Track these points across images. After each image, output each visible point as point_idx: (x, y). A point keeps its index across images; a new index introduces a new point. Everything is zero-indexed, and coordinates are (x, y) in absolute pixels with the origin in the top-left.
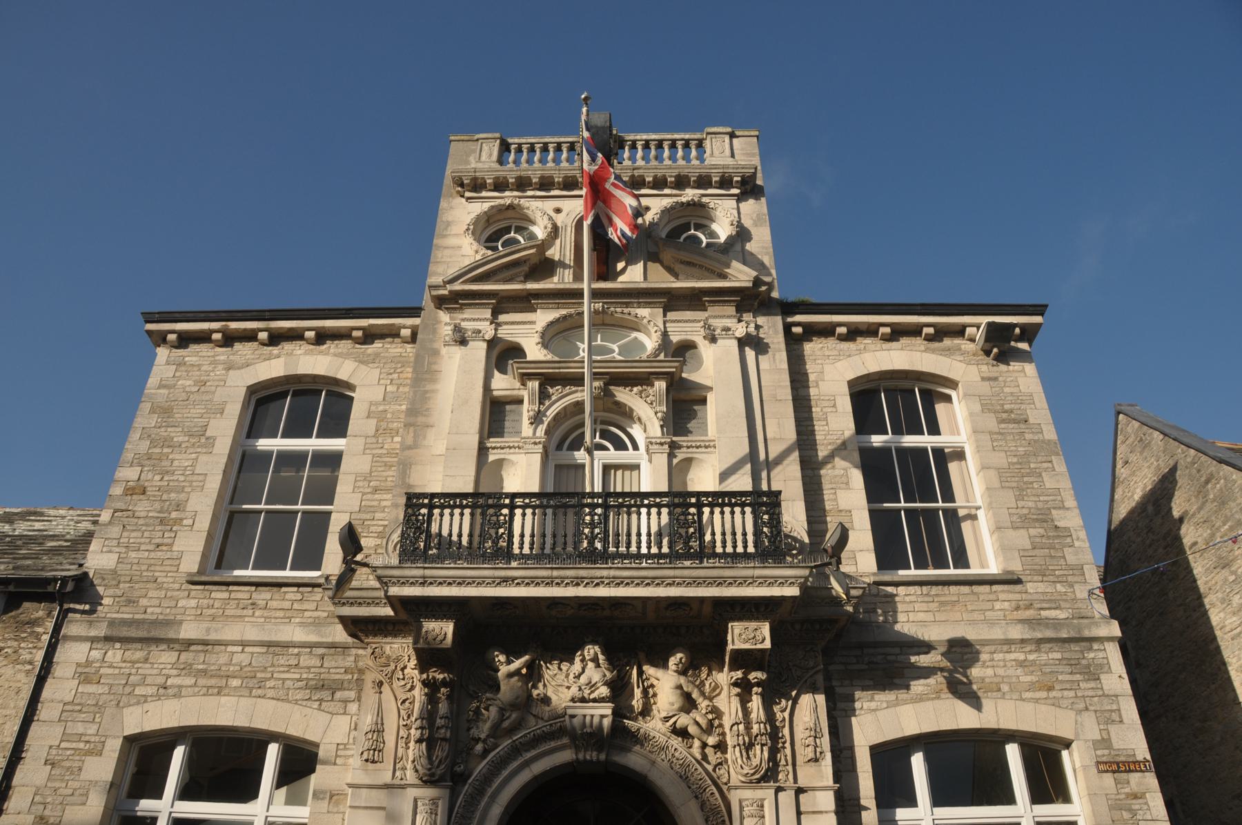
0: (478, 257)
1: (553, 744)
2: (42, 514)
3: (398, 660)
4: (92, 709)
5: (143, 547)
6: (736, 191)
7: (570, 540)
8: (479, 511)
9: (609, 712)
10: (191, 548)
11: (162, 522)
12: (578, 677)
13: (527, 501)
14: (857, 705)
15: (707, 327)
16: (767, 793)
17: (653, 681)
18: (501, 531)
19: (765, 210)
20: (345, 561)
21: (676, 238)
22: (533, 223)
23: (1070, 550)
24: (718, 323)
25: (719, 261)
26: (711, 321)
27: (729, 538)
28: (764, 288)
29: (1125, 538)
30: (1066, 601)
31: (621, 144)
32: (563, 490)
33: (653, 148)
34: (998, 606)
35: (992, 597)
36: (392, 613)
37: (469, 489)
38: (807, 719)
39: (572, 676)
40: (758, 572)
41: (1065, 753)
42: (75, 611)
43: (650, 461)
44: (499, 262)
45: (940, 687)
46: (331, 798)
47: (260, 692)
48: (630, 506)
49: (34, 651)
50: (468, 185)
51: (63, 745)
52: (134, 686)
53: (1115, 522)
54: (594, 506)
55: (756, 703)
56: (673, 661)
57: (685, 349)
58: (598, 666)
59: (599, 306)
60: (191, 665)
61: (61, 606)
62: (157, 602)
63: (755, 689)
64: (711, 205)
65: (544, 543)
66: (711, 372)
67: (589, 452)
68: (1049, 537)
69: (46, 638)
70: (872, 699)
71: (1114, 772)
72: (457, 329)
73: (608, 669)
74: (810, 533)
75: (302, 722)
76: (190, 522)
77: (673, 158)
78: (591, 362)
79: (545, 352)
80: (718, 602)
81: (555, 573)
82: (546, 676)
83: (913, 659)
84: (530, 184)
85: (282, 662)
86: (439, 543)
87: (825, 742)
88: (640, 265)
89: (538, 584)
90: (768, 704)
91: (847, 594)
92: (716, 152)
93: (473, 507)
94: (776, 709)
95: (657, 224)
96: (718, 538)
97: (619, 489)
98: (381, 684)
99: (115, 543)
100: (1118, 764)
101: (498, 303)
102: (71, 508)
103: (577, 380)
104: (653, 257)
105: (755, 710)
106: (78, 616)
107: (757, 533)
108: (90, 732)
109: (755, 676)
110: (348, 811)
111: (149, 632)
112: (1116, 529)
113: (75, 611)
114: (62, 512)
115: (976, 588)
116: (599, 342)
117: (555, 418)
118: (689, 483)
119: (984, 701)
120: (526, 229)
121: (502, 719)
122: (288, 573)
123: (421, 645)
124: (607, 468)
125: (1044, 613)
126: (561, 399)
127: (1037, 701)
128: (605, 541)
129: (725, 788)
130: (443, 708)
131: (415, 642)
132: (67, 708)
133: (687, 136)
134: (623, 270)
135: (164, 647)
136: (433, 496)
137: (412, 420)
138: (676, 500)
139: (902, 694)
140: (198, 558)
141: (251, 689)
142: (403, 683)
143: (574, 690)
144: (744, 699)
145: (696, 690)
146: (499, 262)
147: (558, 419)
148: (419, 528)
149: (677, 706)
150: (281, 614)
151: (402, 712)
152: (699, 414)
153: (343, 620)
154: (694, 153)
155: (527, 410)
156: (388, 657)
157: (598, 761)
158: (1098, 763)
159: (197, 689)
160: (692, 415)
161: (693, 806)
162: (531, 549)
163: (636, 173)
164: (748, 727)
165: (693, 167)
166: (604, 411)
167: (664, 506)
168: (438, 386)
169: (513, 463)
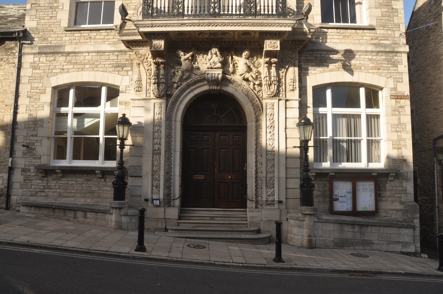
1: (201, 84)
2: (3, 8)
3: (145, 55)
4: (39, 78)
5: (45, 18)
7: (206, 8)
9: (221, 72)
10: (64, 17)
11: (51, 8)
12: (210, 60)
14: (309, 72)
16: (275, 101)
17: (236, 61)
20: (122, 19)
23: (396, 17)
27: (266, 8)
29: (419, 15)
30: (391, 37)
34: (365, 38)
35: (363, 35)
36: (141, 38)
38: (291, 76)
39: (207, 60)
40: (276, 21)
41: (380, 92)
42: (25, 44)
45: (340, 66)
46: (125, 104)
47: (97, 69)
49: (14, 59)
51: (32, 91)
52: (52, 69)
53: (417, 8)
55: (273, 70)
56: (244, 54)
58: (217, 56)
60: (71, 61)
61: (20, 42)
62: (55, 39)
63: (273, 65)
65: (196, 10)
68: (389, 12)
69: (17, 54)
70: (315, 70)
71: (396, 99)
73: (220, 57)
74: (297, 7)
75: (113, 79)
76: (62, 7)
81: (201, 21)
82: (198, 60)
83: (331, 56)
85: (103, 58)
86: (157, 11)
87: (297, 84)
90: (278, 70)
91: (309, 31)
94: (280, 72)
96: (262, 8)
98: (139, 64)
99: (34, 17)
100: (398, 96)
102: (14, 5)
105: (273, 72)
106: (27, 45)
107: (277, 6)
108: (40, 86)
109: (274, 60)
110: (132, 108)
111: (54, 50)
112: (416, 11)
113: (25, 44)
114: (11, 6)
115: (358, 31)
119: (355, 73)
121: (183, 75)
122: (101, 26)
123: (153, 49)
125: (382, 42)
127: (373, 73)
128: (219, 9)
129: (261, 99)
130: (162, 72)
131: (151, 48)
132: (30, 78)
135: (60, 55)
139: (326, 69)
140: (67, 21)
141: (93, 68)
142: (147, 63)
143: (208, 65)
144: (269, 69)
148: (149, 5)
149: (245, 70)
150: (101, 41)
151: (148, 74)
153: (124, 41)
156: (141, 55)
157: (217, 90)
158: (391, 96)
159: (74, 69)
161: (250, 105)
162: (192, 12)
164: (270, 78)
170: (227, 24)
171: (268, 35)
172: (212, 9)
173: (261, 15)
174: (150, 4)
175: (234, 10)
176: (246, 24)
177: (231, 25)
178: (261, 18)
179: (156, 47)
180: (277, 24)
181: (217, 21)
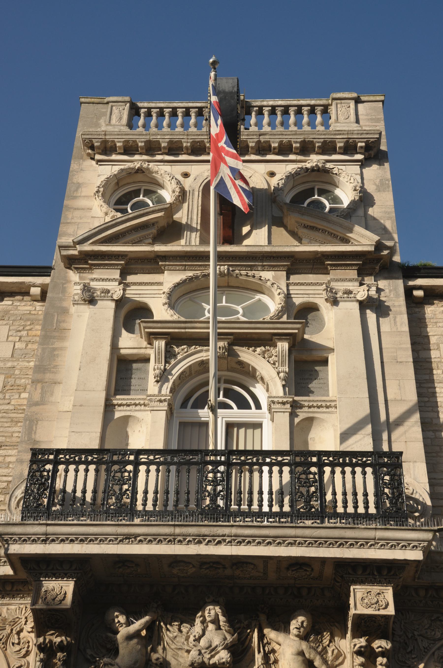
0: (108, 219)
3: (14, 622)
6: (359, 157)
7: (193, 497)
8: (104, 467)
12: (198, 640)
13: (151, 457)
15: (329, 289)
18: (125, 487)
19: (388, 175)
21: (299, 202)
22: (162, 187)
24: (340, 287)
25: (341, 226)
26: (333, 284)
27: (350, 498)
28: (386, 252)
31: (248, 109)
32: (187, 447)
33: (279, 113)
37: (95, 445)
39: (192, 638)
40: (380, 534)
43: (272, 420)
44: (128, 224)
48: (252, 465)
50: (98, 147)
54: (217, 464)
56: (294, 624)
57: (307, 311)
58: (219, 628)
59: (224, 269)
63: (380, 660)
64: (335, 171)
66: (333, 334)
67: (213, 410)
72: (86, 288)
77: (298, 124)
78: (216, 322)
79: (172, 312)
80: (341, 564)
81: (178, 530)
82: (166, 638)
84: (159, 149)
86: (63, 500)
88: (265, 229)
89: (160, 542)
92: (341, 118)
93: (98, 463)
95: (281, 189)
96: (339, 497)
97: (241, 448)
101: (126, 264)
103: (202, 340)
104: (277, 222)
107: (378, 494)
109: (380, 644)
116: (224, 303)
117: (180, 377)
118: (310, 442)
120: (155, 192)
123: (40, 605)
124: (230, 426)
126: (186, 359)
128: (227, 498)
131: (34, 603)
133: (313, 102)
134: (249, 234)
136: (58, 452)
137: (39, 376)
138: (298, 459)
142: (17, 648)
145: (318, 657)
146: (128, 224)
147: (183, 377)
148: (44, 484)
152: (321, 375)
154: (319, 119)
155: (153, 368)
160: (314, 375)
162: (155, 505)
163: (262, 139)
165: (318, 132)
166: (228, 370)
167: (286, 464)
168: (66, 344)
169: (138, 420)
170: (248, 539)
171: (360, 572)
172: (208, 499)
173: (336, 515)
174: (47, 480)
175: (266, 503)
176: (299, 540)
177: (259, 543)
178: (338, 525)
179: (49, 597)
180: (382, 542)
181: (221, 531)
